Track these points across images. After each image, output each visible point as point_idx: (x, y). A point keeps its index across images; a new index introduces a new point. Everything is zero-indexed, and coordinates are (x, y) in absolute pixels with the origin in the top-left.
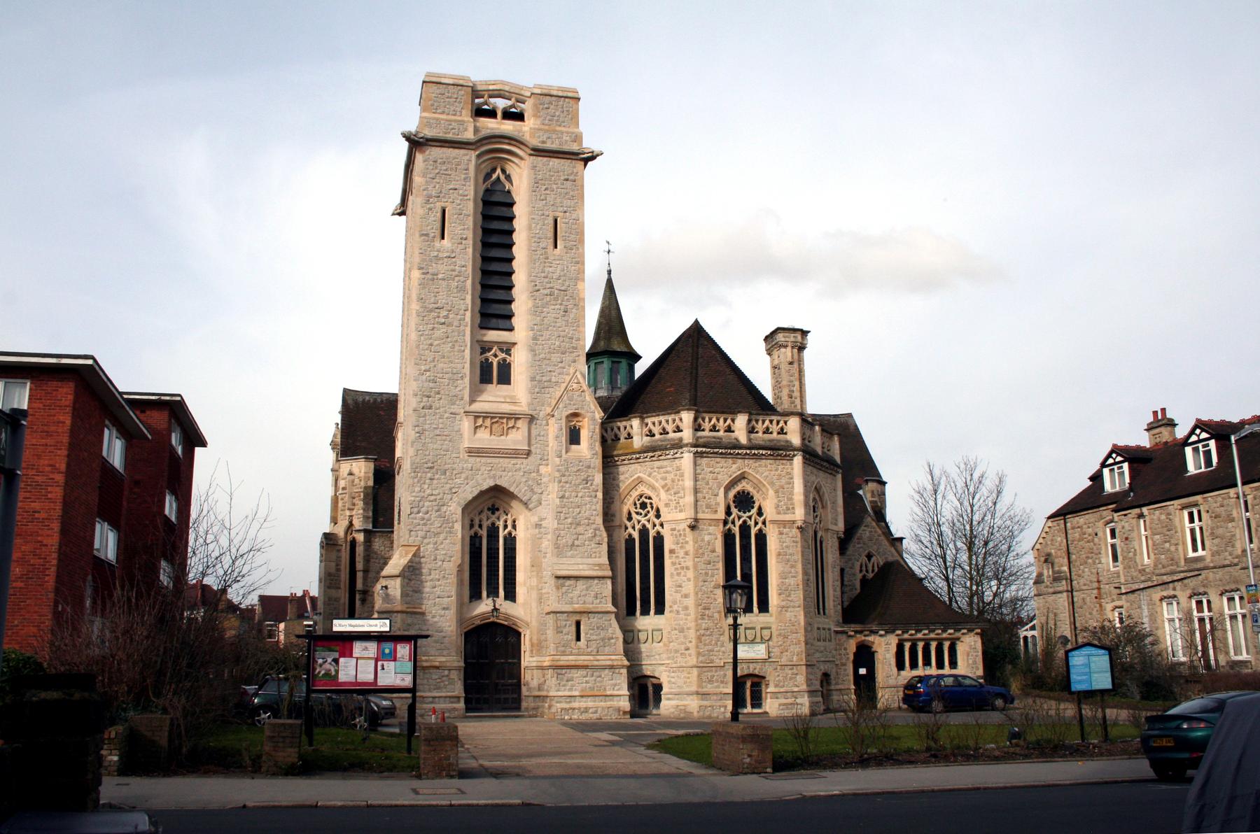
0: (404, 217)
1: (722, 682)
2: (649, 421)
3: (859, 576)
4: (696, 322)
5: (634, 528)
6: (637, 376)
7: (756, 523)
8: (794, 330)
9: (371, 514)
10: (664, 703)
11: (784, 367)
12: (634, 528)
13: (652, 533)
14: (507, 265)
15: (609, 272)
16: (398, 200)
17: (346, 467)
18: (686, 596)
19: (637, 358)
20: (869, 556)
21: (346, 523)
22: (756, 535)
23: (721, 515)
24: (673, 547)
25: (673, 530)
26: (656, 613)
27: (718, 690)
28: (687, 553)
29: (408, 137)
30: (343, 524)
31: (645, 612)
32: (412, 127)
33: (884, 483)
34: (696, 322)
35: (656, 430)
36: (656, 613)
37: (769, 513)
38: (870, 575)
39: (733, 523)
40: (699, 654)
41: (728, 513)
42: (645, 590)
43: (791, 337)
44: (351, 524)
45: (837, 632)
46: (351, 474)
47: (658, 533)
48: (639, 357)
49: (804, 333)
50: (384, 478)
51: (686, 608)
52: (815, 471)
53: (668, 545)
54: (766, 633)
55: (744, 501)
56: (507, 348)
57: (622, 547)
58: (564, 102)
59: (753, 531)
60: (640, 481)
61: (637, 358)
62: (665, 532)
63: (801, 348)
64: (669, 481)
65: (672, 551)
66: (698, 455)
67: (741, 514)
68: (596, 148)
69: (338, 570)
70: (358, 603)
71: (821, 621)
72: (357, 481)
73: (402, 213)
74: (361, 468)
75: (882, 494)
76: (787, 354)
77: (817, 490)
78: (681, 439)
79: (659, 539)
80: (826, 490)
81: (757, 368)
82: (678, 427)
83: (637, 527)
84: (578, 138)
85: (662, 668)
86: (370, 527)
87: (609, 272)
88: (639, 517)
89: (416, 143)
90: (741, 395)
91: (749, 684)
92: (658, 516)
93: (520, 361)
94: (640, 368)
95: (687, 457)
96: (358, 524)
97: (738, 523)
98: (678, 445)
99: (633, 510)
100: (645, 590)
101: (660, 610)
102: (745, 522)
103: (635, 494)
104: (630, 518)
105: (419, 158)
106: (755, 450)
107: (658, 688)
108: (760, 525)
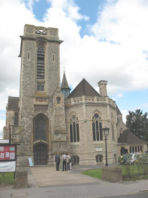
0: (21, 58)
1: (93, 157)
2: (75, 98)
3: (119, 133)
4: (84, 78)
5: (72, 123)
6: (70, 93)
7: (99, 121)
8: (104, 81)
9: (14, 122)
10: (80, 162)
11: (102, 89)
12: (72, 123)
13: (76, 123)
14: (43, 68)
15: (64, 72)
16: (19, 54)
17: (9, 113)
18: (84, 137)
19: (70, 89)
20: (121, 129)
21: (9, 124)
22: (99, 123)
23: (92, 119)
24: (81, 126)
25: (81, 122)
26: (97, 140)
27: (91, 159)
28: (84, 128)
29: (21, 37)
30: (8, 124)
31: (75, 141)
32: (22, 34)
33: (122, 114)
34: (84, 78)
35: (76, 100)
36: (97, 140)
37: (103, 118)
38: (122, 133)
39: (94, 121)
40: (88, 150)
41: (93, 118)
42: (97, 133)
43: (104, 82)
44: (10, 124)
45: (117, 145)
46: (10, 114)
47: (77, 123)
48: (71, 89)
49: (106, 82)
50: (17, 115)
51: (84, 140)
52: (111, 109)
53: (80, 126)
54: (102, 145)
55: (96, 116)
56: (44, 83)
57: (69, 126)
58: (55, 31)
59: (99, 122)
60: (73, 112)
61: (70, 89)
62: (79, 123)
63: (106, 85)
64: (80, 112)
65: (81, 127)
66: (86, 106)
67: (97, 119)
68: (62, 40)
69: (7, 134)
70: (11, 141)
71: (114, 142)
72: (11, 115)
73: (20, 56)
74: (12, 113)
75: (122, 117)
76: (102, 86)
77: (112, 114)
78: (82, 102)
79: (78, 125)
80: (113, 113)
81: (97, 89)
82: (81, 99)
83: (73, 122)
84: (58, 38)
85: (79, 154)
86: (14, 125)
87: (64, 72)
88: (73, 120)
89: (23, 38)
90: (93, 93)
91: (99, 157)
92: (77, 119)
93: (46, 85)
94: (71, 92)
95: (84, 106)
96: (11, 124)
97: (95, 121)
98: (82, 104)
99: (71, 118)
100: (97, 133)
101: (78, 141)
102: (97, 120)
103: (72, 115)
104: (71, 120)
105: (24, 41)
106: (98, 105)
107: (78, 158)
108: (100, 121)
